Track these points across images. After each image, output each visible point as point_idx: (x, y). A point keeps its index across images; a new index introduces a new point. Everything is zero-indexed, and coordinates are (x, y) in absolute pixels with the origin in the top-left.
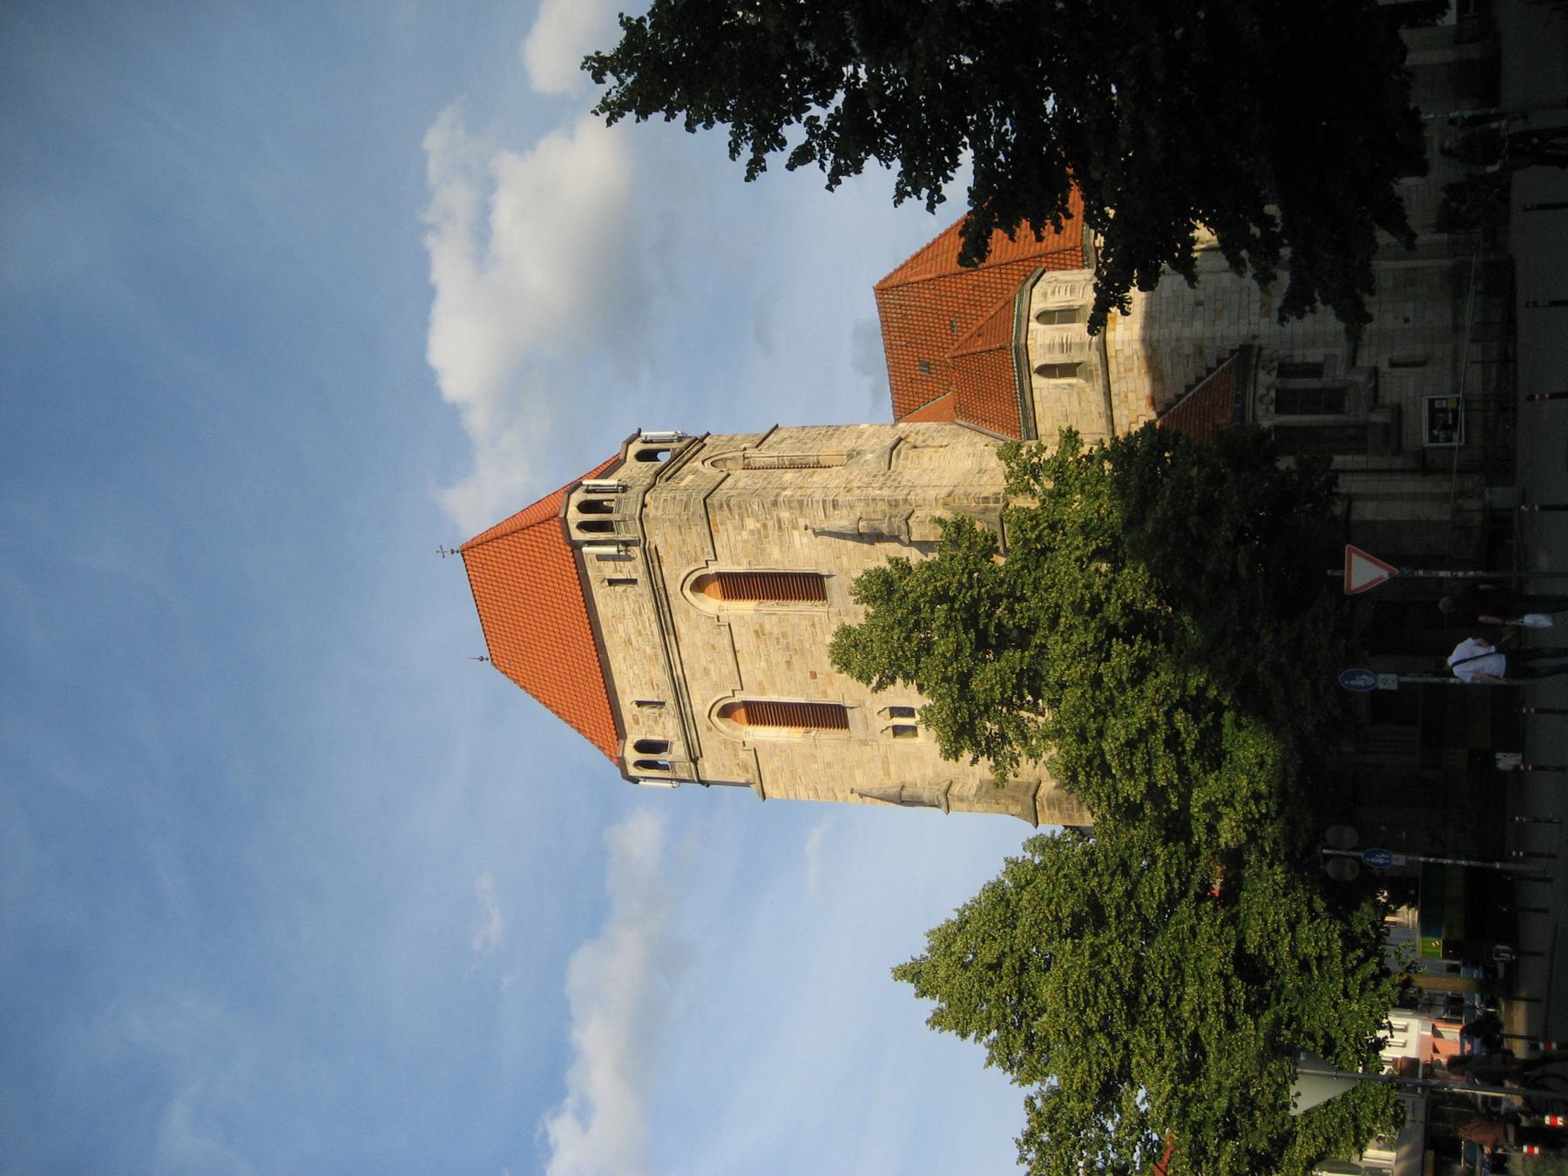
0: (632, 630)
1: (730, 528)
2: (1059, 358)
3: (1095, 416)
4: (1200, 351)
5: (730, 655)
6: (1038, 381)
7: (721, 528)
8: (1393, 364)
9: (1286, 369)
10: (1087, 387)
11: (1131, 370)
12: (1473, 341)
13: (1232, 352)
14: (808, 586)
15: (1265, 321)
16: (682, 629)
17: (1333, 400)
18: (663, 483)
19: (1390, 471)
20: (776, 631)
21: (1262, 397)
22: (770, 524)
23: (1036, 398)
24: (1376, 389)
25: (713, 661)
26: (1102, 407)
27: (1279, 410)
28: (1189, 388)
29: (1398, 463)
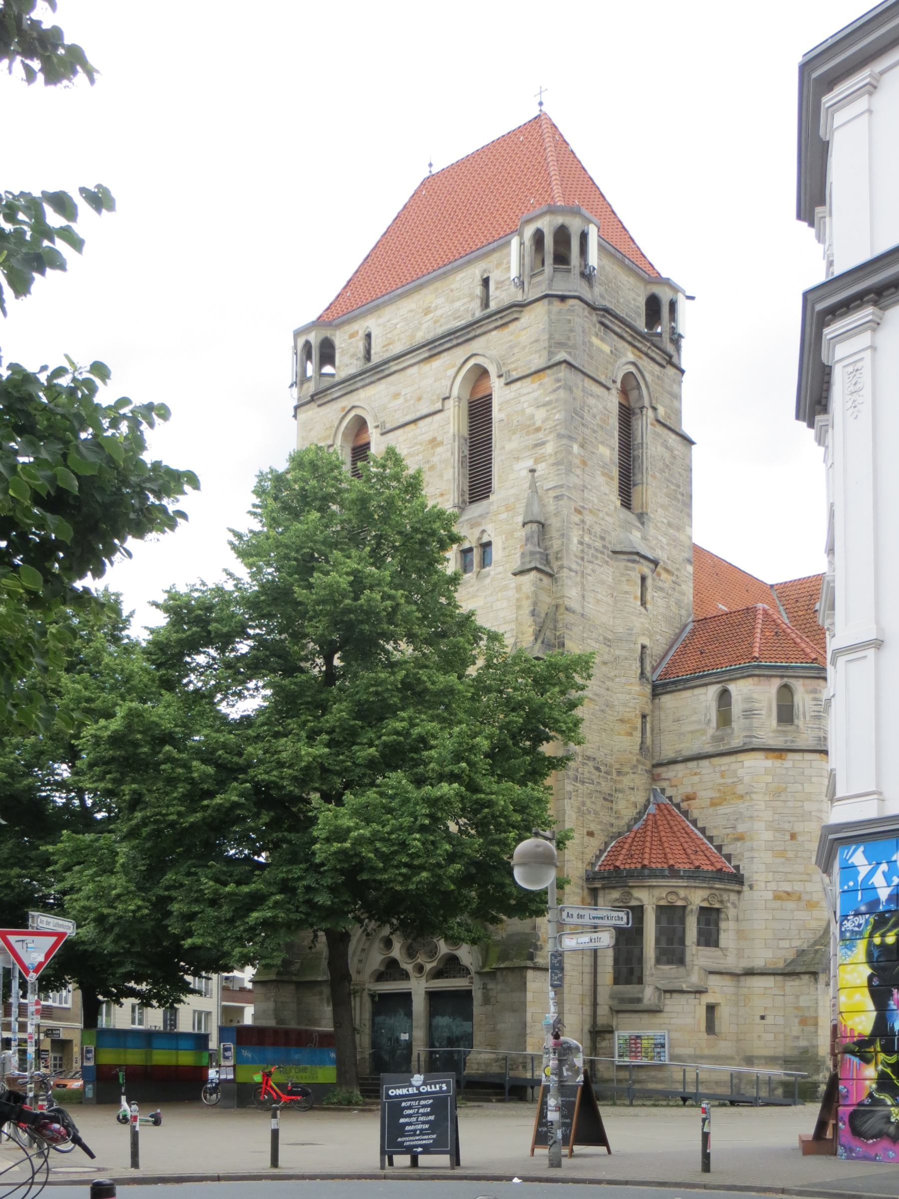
0: (439, 313)
1: (535, 395)
2: (737, 708)
3: (678, 747)
4: (740, 838)
5: (409, 418)
6: (713, 691)
7: (535, 386)
8: (711, 1009)
9: (710, 917)
10: (707, 738)
11: (723, 777)
12: (70, 1042)
13: (737, 868)
14: (478, 485)
15: (770, 895)
16: (437, 363)
17: (672, 952)
18: (594, 318)
19: (595, 1004)
20: (435, 459)
21: (676, 894)
22: (541, 435)
23: (697, 691)
24: (682, 992)
25: (406, 401)
26: (687, 753)
27: (661, 910)
28: (703, 830)
29: (603, 1011)
